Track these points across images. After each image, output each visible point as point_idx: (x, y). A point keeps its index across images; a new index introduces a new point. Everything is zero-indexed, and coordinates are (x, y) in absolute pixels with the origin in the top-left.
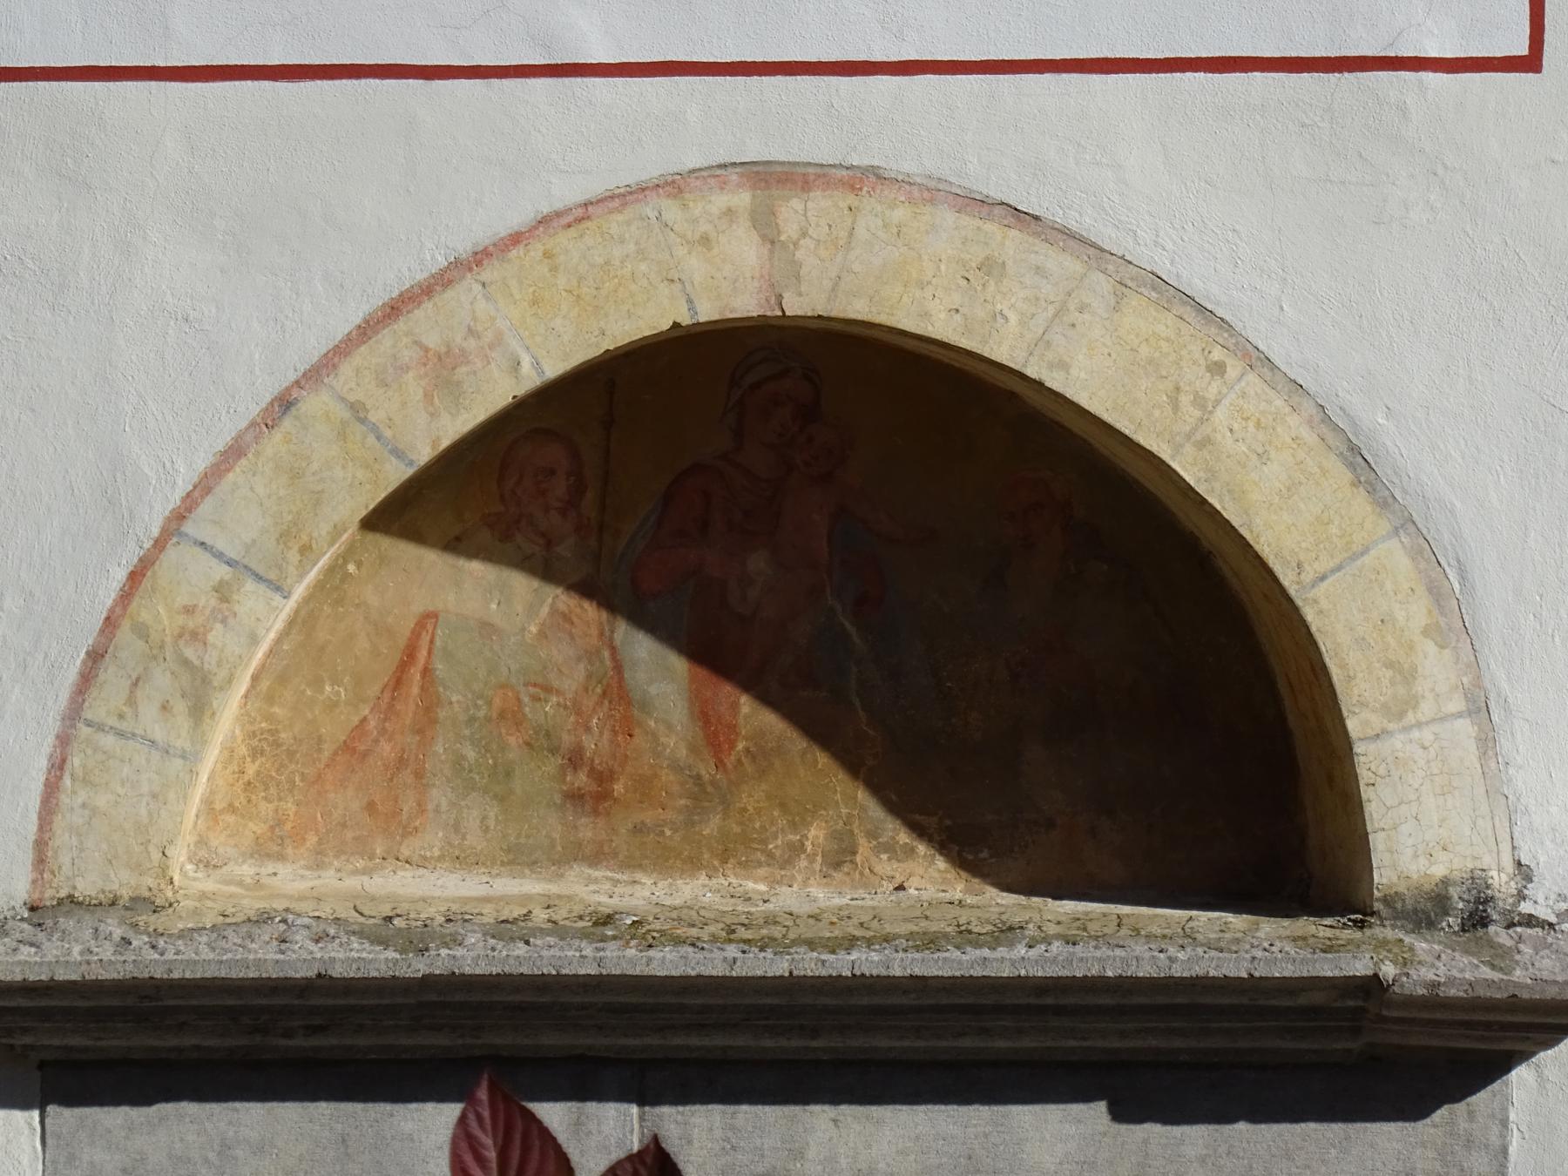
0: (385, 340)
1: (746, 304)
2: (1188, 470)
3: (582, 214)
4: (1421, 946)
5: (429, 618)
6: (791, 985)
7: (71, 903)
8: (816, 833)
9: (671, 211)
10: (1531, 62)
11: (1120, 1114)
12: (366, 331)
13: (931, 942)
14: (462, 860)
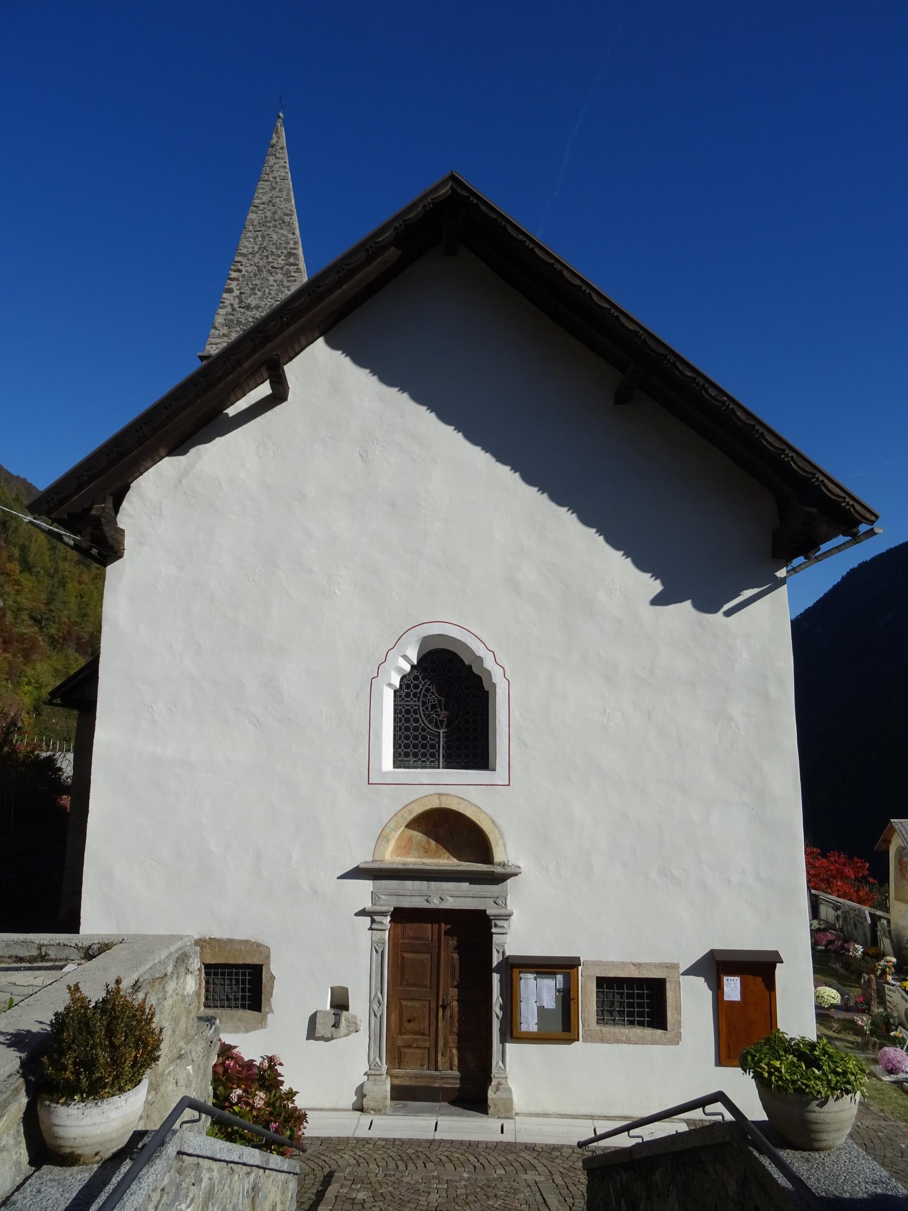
0: (405, 809)
1: (438, 806)
2: (477, 822)
3: (423, 798)
4: (498, 868)
5: (412, 835)
6: (439, 870)
7: (376, 861)
8: (446, 856)
9: (431, 798)
10: (509, 785)
11: (470, 884)
12: (403, 808)
13: (453, 866)
14: (415, 857)
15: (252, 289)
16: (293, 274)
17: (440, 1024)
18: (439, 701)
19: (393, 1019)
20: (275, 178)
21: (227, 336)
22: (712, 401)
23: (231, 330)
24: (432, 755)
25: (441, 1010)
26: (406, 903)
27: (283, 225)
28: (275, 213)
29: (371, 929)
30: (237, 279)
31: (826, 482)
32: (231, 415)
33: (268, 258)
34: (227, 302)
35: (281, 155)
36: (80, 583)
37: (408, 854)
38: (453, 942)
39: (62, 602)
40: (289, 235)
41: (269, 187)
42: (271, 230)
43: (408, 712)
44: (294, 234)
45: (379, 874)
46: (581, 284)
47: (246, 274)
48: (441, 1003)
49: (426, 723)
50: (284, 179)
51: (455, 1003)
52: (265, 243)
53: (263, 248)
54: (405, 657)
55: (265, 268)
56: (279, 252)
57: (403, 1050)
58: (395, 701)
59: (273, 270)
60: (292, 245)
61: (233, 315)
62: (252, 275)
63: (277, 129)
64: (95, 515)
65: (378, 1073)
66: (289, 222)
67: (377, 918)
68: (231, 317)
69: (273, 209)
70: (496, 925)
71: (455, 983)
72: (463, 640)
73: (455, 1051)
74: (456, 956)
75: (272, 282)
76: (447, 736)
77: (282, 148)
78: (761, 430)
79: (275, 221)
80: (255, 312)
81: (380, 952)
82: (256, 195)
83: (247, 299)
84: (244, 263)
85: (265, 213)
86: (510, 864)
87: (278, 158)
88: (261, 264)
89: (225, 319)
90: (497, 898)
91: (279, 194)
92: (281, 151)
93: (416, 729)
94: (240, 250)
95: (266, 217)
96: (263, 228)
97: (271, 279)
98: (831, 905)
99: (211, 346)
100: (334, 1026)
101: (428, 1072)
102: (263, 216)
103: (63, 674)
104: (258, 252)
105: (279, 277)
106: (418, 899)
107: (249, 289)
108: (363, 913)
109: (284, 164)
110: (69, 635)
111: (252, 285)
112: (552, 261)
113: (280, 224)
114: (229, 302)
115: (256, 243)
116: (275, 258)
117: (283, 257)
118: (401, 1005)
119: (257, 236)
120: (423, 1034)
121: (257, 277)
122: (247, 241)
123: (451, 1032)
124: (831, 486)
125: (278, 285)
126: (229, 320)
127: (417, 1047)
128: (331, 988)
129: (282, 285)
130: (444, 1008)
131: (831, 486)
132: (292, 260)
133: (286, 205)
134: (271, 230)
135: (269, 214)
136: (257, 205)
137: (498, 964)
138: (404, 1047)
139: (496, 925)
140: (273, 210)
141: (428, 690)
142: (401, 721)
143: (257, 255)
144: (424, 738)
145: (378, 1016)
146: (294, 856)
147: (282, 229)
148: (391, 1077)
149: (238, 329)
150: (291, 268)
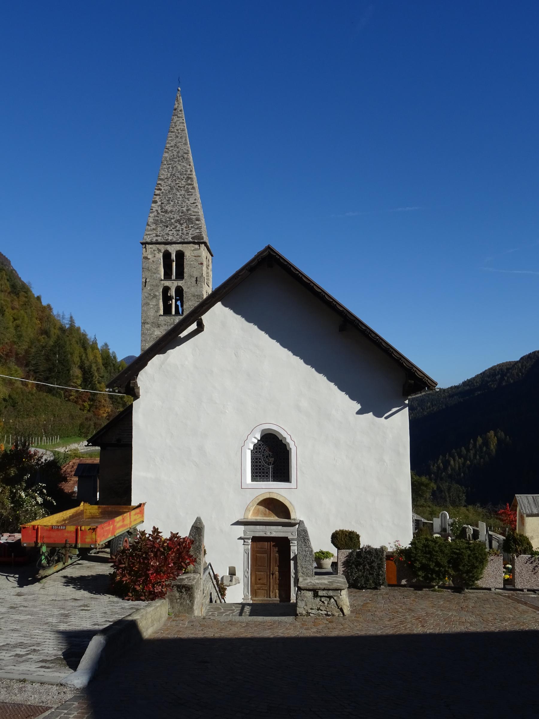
1: (269, 497)
14: (260, 517)
15: (168, 201)
16: (190, 190)
17: (271, 581)
18: (269, 454)
19: (253, 579)
20: (177, 130)
21: (155, 230)
22: (373, 338)
23: (157, 226)
24: (267, 476)
25: (271, 575)
26: (257, 535)
27: (184, 160)
28: (178, 152)
29: (244, 544)
30: (159, 195)
31: (417, 371)
32: (182, 337)
33: (176, 181)
34: (154, 209)
35: (180, 115)
36: (13, 309)
37: (258, 515)
38: (276, 549)
39: (5, 328)
40: (187, 166)
41: (175, 136)
42: (177, 163)
43: (257, 459)
44: (190, 165)
45: (247, 523)
46: (321, 291)
47: (164, 191)
48: (271, 573)
49: (264, 463)
50: (183, 130)
51: (277, 573)
52: (173, 171)
53: (173, 175)
54: (255, 438)
55: (175, 187)
56: (182, 177)
57: (257, 591)
58: (251, 454)
59: (179, 188)
60: (189, 172)
61: (158, 217)
62: (167, 192)
63: (177, 98)
64: (132, 387)
65: (247, 598)
66: (187, 158)
67: (246, 540)
68: (157, 218)
69: (178, 150)
70: (292, 543)
71: (277, 565)
72: (278, 431)
73: (277, 591)
74: (277, 555)
75: (179, 196)
76: (274, 469)
77: (181, 111)
78: (392, 350)
79: (179, 157)
80: (170, 214)
81: (247, 553)
82: (167, 141)
83: (165, 207)
84: (162, 185)
85: (173, 153)
86: (297, 519)
87: (179, 117)
88: (172, 185)
89: (154, 220)
90: (292, 532)
91: (180, 140)
92: (180, 112)
93: (260, 466)
94: (160, 176)
95: (173, 155)
96: (172, 162)
97: (178, 194)
98: (497, 540)
99: (147, 236)
100: (230, 581)
101: (266, 599)
102: (172, 154)
103: (7, 381)
104: (170, 178)
105: (183, 192)
106: (262, 533)
107: (166, 201)
108: (240, 538)
109: (183, 121)
110: (11, 352)
111: (168, 198)
112: (309, 282)
113: (182, 159)
114: (155, 209)
115: (168, 172)
116: (180, 181)
117: (184, 180)
118: (256, 573)
119: (169, 168)
120: (265, 585)
121: (170, 193)
122: (163, 171)
123: (276, 584)
124: (419, 373)
125: (182, 198)
126: (156, 220)
127: (262, 590)
128: (229, 567)
129: (185, 197)
130: (273, 574)
131: (419, 373)
132: (189, 182)
133: (185, 147)
134: (177, 163)
135: (175, 153)
136: (168, 148)
137: (293, 557)
138: (257, 589)
139: (292, 543)
140: (177, 151)
141: (264, 450)
142: (254, 463)
143: (170, 179)
144: (263, 469)
145: (247, 577)
146: (213, 517)
147: (183, 162)
148: (252, 600)
149: (161, 225)
150: (189, 187)
